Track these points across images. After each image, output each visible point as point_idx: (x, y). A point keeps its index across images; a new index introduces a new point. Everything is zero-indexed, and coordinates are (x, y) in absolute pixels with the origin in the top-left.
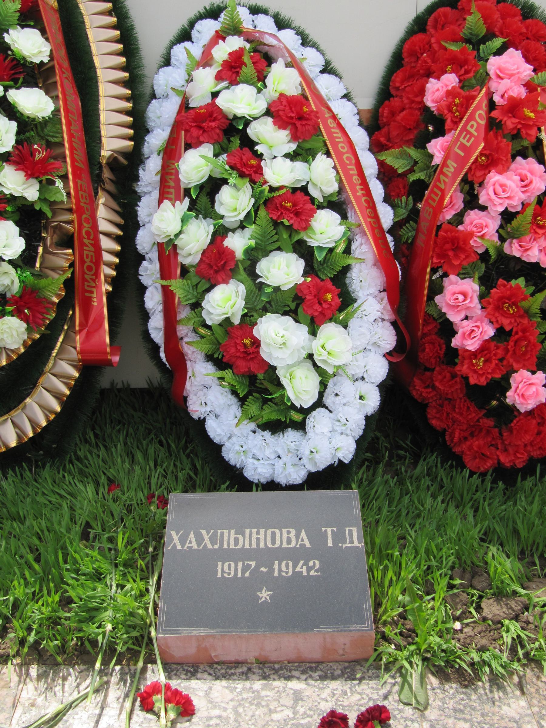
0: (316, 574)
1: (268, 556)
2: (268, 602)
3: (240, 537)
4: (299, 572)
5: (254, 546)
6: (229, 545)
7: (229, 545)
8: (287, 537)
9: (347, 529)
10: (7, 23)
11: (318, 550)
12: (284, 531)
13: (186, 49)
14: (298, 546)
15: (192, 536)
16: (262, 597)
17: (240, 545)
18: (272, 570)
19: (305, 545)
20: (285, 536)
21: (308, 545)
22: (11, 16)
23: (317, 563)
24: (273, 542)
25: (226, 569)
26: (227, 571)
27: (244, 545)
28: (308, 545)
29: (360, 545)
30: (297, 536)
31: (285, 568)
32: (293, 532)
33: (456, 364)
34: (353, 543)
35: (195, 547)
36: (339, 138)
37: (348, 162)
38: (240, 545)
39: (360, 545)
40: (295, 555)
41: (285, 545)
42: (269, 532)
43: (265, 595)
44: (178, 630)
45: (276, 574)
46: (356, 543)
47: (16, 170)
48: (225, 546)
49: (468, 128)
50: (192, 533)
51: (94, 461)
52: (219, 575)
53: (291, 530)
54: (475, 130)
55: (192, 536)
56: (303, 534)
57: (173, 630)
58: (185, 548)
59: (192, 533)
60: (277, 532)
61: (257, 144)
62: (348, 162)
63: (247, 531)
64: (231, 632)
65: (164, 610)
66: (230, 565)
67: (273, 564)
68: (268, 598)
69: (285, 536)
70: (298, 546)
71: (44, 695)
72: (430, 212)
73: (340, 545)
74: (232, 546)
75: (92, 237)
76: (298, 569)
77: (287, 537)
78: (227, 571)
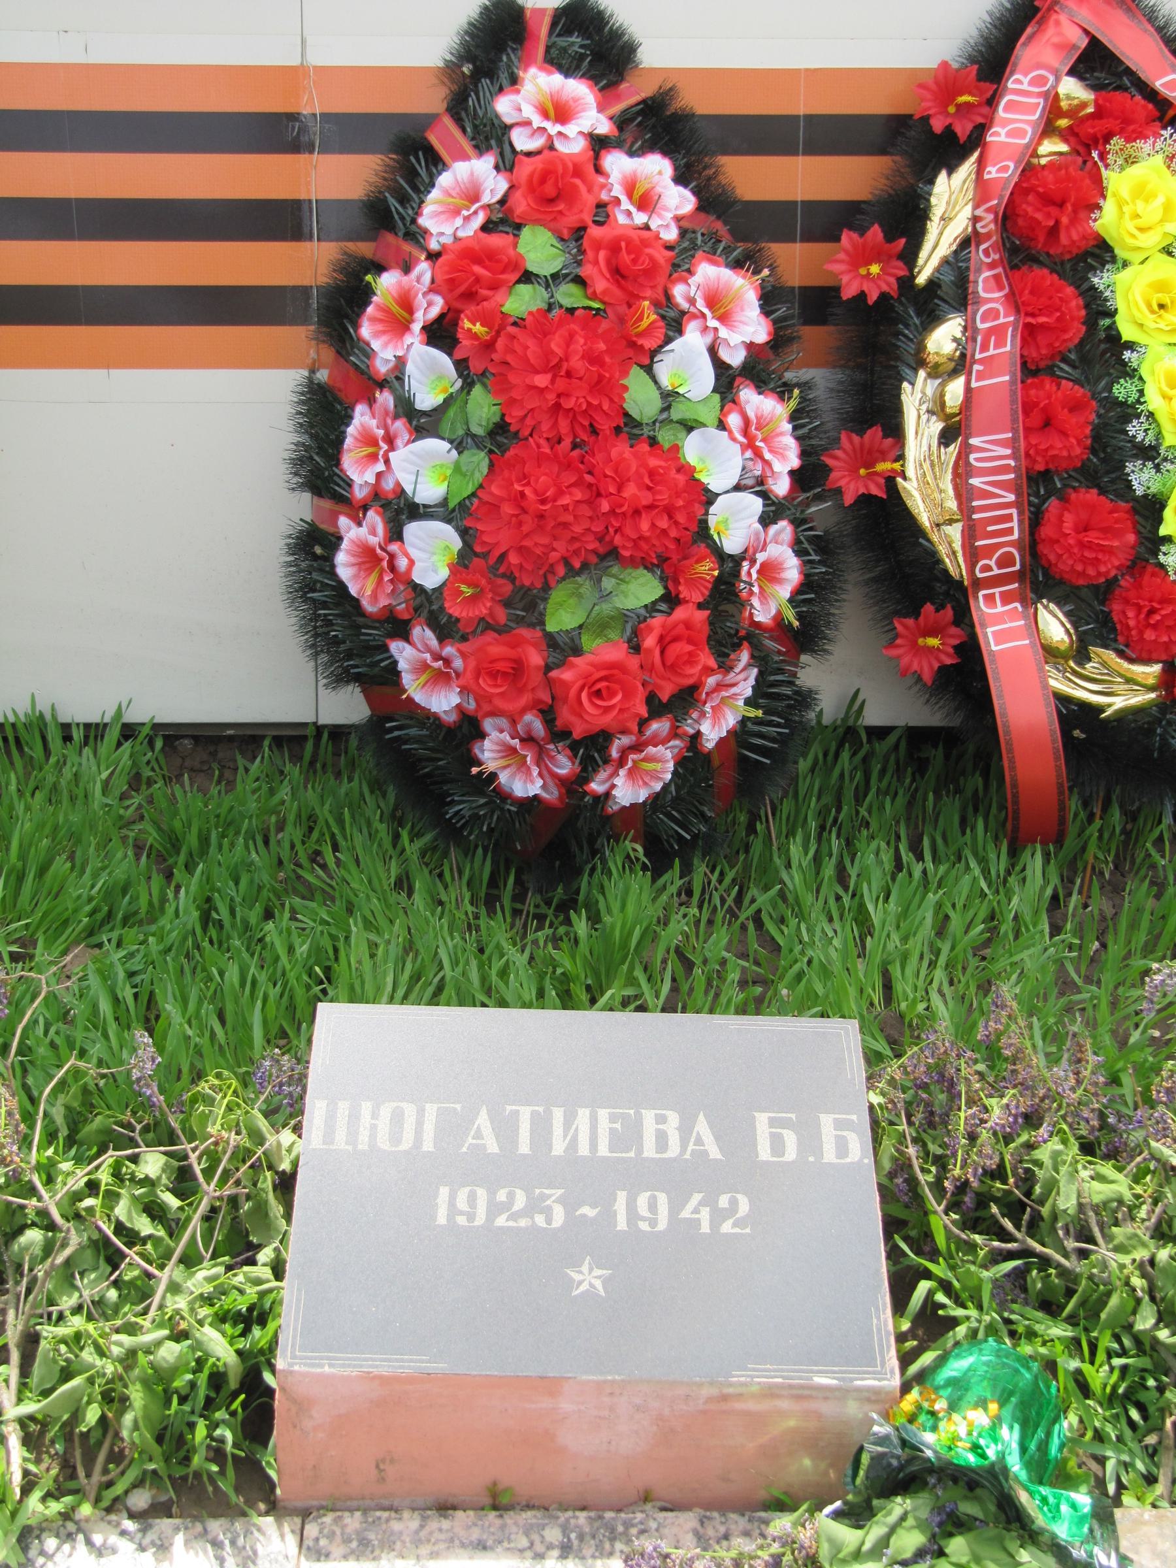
0: (737, 1230)
2: (598, 1295)
14: (687, 1156)
16: (580, 1283)
19: (706, 1153)
21: (714, 1152)
23: (744, 1206)
24: (396, 1139)
25: (457, 1206)
26: (648, 1215)
28: (714, 1152)
30: (686, 1130)
31: (654, 1211)
32: (673, 1118)
33: (916, 613)
34: (818, 1150)
40: (677, 1179)
42: (386, 1111)
43: (589, 1278)
44: (879, 1330)
45: (622, 1224)
46: (603, 1150)
50: (701, 1117)
52: (442, 1219)
55: (483, 1120)
56: (702, 1127)
58: (464, 1149)
59: (701, 1117)
60: (410, 1110)
61: (949, 174)
65: (297, 1312)
68: (583, 1288)
70: (687, 1156)
71: (81, 1537)
76: (686, 1214)
78: (648, 1215)
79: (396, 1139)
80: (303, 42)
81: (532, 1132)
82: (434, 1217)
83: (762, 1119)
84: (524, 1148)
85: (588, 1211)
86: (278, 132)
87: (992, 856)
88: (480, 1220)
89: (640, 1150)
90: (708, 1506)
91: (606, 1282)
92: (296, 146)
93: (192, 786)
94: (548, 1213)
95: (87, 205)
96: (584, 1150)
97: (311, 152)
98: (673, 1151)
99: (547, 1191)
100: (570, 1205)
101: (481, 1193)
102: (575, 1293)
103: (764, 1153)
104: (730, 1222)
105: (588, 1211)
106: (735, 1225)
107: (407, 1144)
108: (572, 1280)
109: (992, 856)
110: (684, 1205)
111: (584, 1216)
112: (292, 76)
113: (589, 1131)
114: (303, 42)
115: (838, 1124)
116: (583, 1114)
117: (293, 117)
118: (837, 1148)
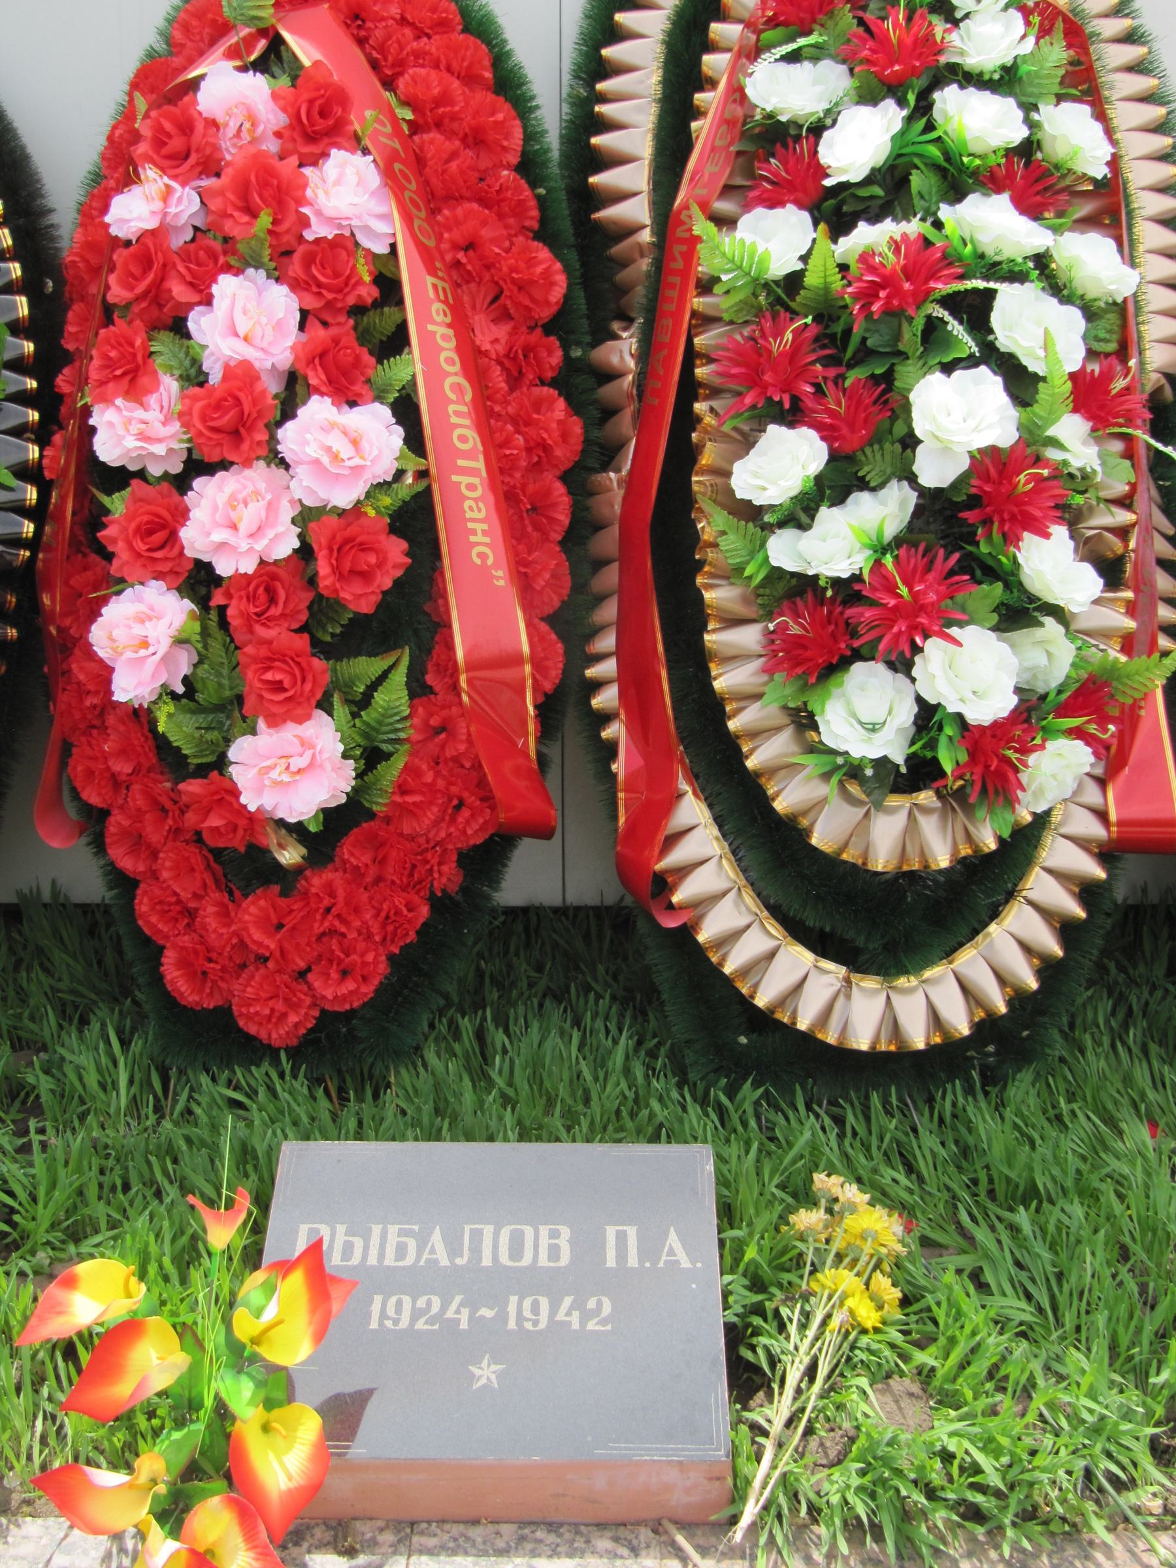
3: (358, 1243)
4: (561, 1323)
9: (467, 1228)
10: (1035, 90)
11: (584, 1276)
12: (544, 1231)
13: (635, 194)
15: (437, 1237)
17: (356, 1260)
18: (503, 1317)
19: (436, 1261)
20: (544, 1242)
22: (1048, 76)
26: (527, 1313)
27: (382, 1255)
28: (685, 1263)
31: (526, 1312)
35: (444, 1262)
36: (457, 413)
37: (453, 397)
38: (356, 1260)
41: (543, 1261)
45: (512, 1324)
48: (487, 1261)
52: (374, 1325)
55: (437, 1237)
57: (649, 1449)
58: (661, 1264)
62: (453, 397)
63: (376, 1230)
66: (399, 1303)
67: (506, 1302)
69: (544, 1242)
73: (699, 1265)
74: (390, 1260)
76: (561, 1316)
77: (547, 1244)
84: (611, 1262)
85: (486, 1313)
87: (1050, 1185)
88: (404, 1323)
90: (523, 1524)
93: (630, 1027)
96: (487, 1261)
98: (409, 1260)
101: (407, 1300)
102: (476, 1386)
104: (423, 1320)
105: (486, 1313)
106: (426, 1323)
108: (473, 1375)
109: (1050, 1185)
111: (483, 1317)
115: (401, 1233)
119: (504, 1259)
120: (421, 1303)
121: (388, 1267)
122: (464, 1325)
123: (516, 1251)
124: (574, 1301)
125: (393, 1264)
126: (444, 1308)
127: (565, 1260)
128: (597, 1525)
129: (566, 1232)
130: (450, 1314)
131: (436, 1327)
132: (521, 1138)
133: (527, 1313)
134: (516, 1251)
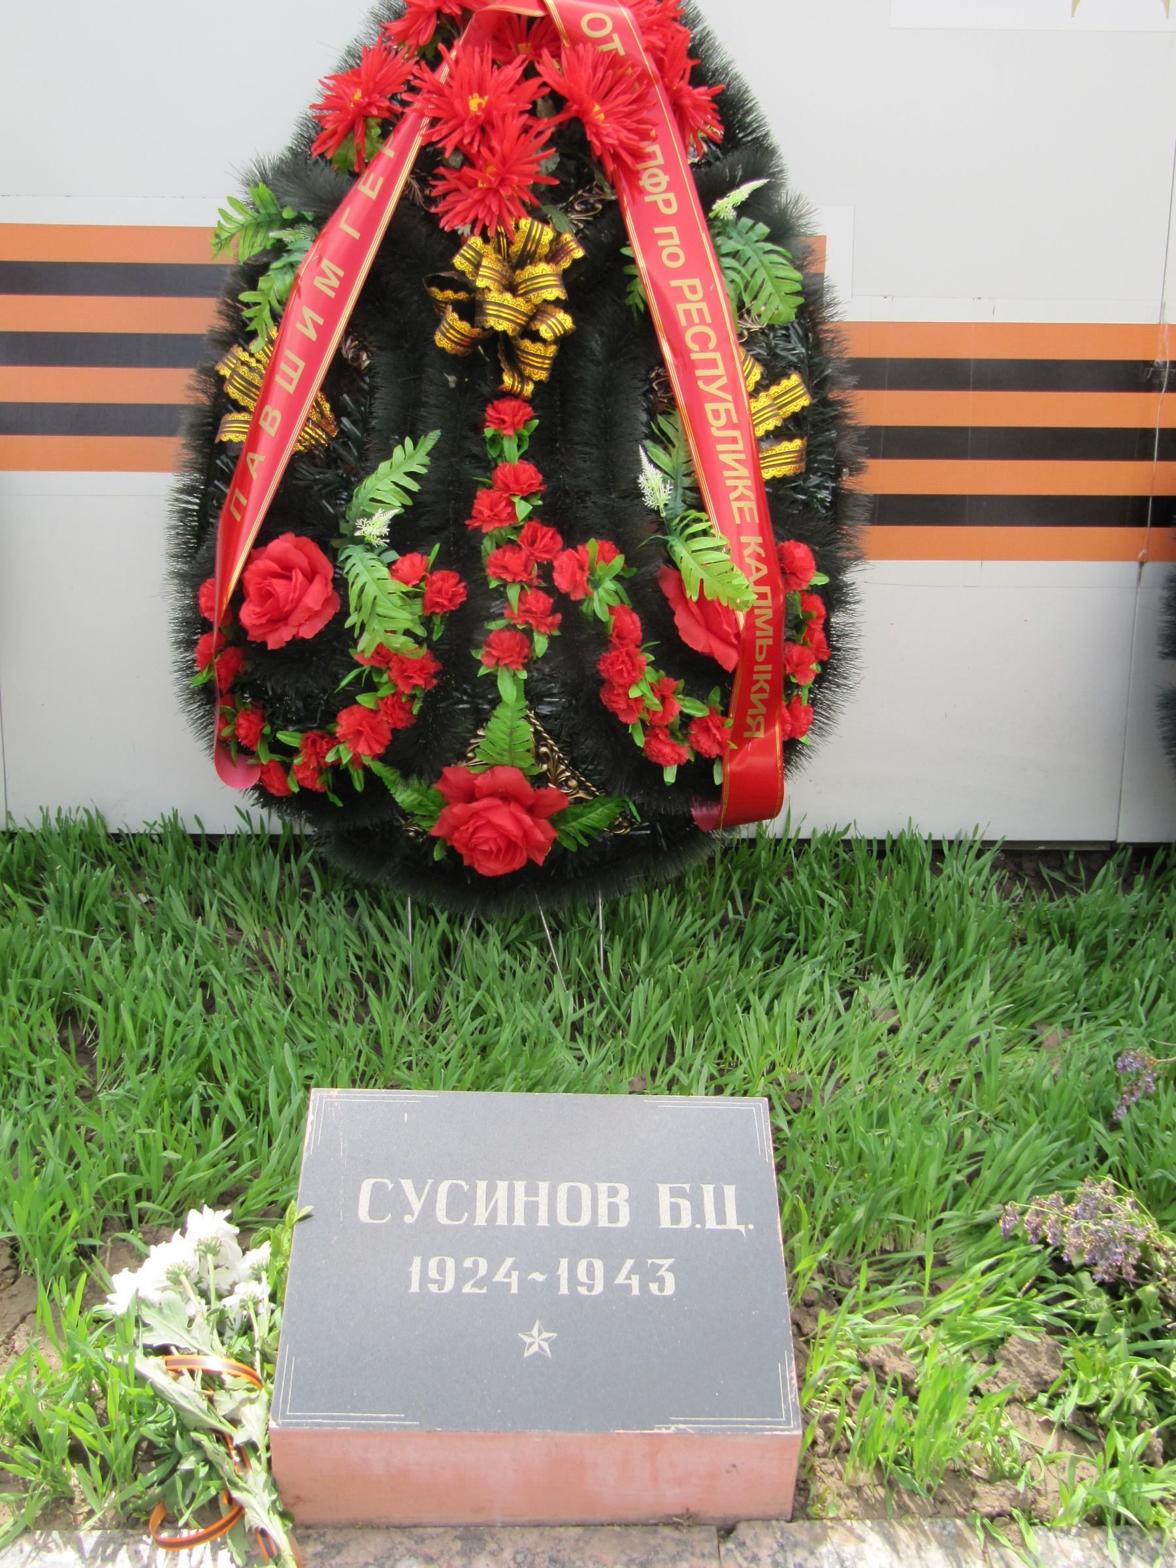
1: (540, 1246)
4: (621, 1285)
5: (519, 1220)
6: (511, 1218)
7: (511, 1218)
8: (607, 1204)
12: (603, 1187)
18: (553, 1281)
20: (603, 1201)
24: (574, 1214)
25: (434, 1275)
26: (582, 1277)
29: (742, 1228)
31: (590, 1277)
34: (703, 1222)
39: (742, 1228)
41: (603, 1222)
43: (537, 1341)
45: (564, 1290)
46: (732, 1223)
47: (220, 312)
49: (696, 282)
51: (749, 1031)
52: (415, 1287)
53: (618, 1185)
54: (680, 289)
60: (585, 1189)
64: (388, 1419)
66: (590, 1267)
69: (603, 1201)
72: (274, 419)
75: (712, 345)
76: (620, 1280)
78: (437, 1277)
79: (574, 1214)
80: (1163, 306)
81: (738, 1206)
82: (558, 1288)
83: (664, 1190)
85: (538, 1277)
86: (1135, 376)
88: (449, 1286)
89: (472, 1218)
91: (552, 1344)
92: (1150, 386)
94: (661, 1281)
95: (84, 408)
97: (1160, 390)
99: (658, 1261)
100: (523, 1267)
102: (526, 1354)
103: (665, 1222)
105: (538, 1277)
107: (585, 1220)
110: (619, 1269)
112: (1150, 332)
113: (548, 1202)
114: (1163, 306)
115: (675, 1193)
116: (502, 1186)
117: (1148, 364)
118: (672, 1215)
119: (563, 1220)
120: (468, 1263)
121: (712, 1231)
122: (514, 1290)
123: (574, 1213)
124: (514, 1263)
125: (607, 1225)
126: (493, 1269)
127: (624, 1221)
128: (671, 1522)
129: (624, 1191)
130: (499, 1277)
131: (484, 1291)
132: (353, 1083)
133: (582, 1277)
134: (574, 1213)
